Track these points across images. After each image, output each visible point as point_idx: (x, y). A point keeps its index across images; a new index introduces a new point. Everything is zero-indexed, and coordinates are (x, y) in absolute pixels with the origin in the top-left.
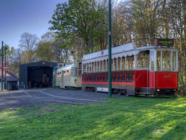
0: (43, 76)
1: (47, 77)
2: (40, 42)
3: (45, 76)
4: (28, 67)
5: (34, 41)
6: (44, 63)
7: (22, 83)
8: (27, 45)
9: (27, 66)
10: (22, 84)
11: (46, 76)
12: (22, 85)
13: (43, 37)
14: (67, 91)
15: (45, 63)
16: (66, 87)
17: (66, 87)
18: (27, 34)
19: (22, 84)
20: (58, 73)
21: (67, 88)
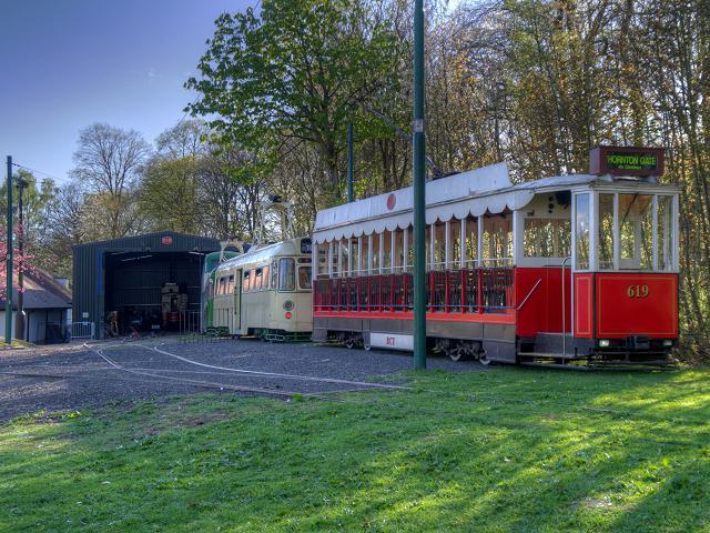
0: (166, 290)
1: (181, 292)
2: (154, 161)
3: (171, 290)
4: (108, 255)
5: (130, 156)
6: (167, 240)
7: (85, 315)
8: (101, 169)
9: (103, 250)
10: (85, 320)
11: (176, 289)
12: (85, 323)
13: (163, 142)
14: (254, 346)
15: (170, 240)
16: (251, 331)
17: (251, 331)
18: (103, 129)
19: (85, 320)
20: (222, 280)
21: (256, 335)
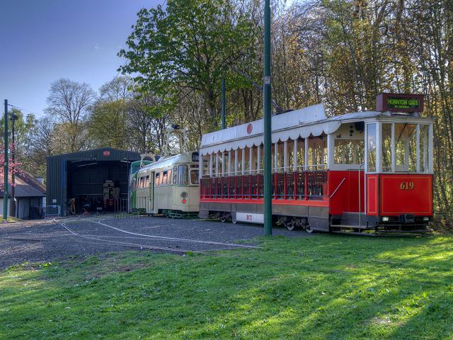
0: (106, 185)
1: (115, 186)
2: (98, 103)
3: (109, 185)
4: (69, 163)
5: (83, 99)
6: (107, 153)
7: (55, 201)
8: (65, 108)
9: (66, 159)
10: (54, 204)
11: (112, 185)
12: (54, 206)
13: (104, 91)
14: (162, 221)
15: (109, 153)
16: (160, 211)
17: (160, 211)
18: (66, 82)
19: (54, 204)
20: (142, 178)
21: (163, 214)
